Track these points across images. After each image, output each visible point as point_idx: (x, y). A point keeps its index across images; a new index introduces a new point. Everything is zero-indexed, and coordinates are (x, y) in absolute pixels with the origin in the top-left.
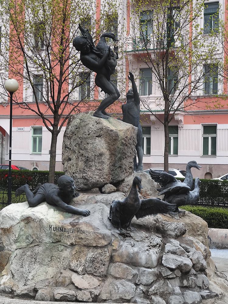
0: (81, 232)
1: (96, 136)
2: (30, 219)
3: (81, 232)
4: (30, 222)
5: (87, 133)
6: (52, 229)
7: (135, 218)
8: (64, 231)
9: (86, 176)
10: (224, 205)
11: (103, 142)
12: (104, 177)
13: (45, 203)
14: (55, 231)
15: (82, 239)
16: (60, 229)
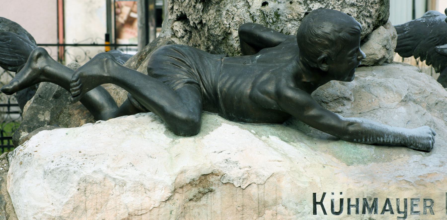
8: (380, 210)
16: (365, 205)
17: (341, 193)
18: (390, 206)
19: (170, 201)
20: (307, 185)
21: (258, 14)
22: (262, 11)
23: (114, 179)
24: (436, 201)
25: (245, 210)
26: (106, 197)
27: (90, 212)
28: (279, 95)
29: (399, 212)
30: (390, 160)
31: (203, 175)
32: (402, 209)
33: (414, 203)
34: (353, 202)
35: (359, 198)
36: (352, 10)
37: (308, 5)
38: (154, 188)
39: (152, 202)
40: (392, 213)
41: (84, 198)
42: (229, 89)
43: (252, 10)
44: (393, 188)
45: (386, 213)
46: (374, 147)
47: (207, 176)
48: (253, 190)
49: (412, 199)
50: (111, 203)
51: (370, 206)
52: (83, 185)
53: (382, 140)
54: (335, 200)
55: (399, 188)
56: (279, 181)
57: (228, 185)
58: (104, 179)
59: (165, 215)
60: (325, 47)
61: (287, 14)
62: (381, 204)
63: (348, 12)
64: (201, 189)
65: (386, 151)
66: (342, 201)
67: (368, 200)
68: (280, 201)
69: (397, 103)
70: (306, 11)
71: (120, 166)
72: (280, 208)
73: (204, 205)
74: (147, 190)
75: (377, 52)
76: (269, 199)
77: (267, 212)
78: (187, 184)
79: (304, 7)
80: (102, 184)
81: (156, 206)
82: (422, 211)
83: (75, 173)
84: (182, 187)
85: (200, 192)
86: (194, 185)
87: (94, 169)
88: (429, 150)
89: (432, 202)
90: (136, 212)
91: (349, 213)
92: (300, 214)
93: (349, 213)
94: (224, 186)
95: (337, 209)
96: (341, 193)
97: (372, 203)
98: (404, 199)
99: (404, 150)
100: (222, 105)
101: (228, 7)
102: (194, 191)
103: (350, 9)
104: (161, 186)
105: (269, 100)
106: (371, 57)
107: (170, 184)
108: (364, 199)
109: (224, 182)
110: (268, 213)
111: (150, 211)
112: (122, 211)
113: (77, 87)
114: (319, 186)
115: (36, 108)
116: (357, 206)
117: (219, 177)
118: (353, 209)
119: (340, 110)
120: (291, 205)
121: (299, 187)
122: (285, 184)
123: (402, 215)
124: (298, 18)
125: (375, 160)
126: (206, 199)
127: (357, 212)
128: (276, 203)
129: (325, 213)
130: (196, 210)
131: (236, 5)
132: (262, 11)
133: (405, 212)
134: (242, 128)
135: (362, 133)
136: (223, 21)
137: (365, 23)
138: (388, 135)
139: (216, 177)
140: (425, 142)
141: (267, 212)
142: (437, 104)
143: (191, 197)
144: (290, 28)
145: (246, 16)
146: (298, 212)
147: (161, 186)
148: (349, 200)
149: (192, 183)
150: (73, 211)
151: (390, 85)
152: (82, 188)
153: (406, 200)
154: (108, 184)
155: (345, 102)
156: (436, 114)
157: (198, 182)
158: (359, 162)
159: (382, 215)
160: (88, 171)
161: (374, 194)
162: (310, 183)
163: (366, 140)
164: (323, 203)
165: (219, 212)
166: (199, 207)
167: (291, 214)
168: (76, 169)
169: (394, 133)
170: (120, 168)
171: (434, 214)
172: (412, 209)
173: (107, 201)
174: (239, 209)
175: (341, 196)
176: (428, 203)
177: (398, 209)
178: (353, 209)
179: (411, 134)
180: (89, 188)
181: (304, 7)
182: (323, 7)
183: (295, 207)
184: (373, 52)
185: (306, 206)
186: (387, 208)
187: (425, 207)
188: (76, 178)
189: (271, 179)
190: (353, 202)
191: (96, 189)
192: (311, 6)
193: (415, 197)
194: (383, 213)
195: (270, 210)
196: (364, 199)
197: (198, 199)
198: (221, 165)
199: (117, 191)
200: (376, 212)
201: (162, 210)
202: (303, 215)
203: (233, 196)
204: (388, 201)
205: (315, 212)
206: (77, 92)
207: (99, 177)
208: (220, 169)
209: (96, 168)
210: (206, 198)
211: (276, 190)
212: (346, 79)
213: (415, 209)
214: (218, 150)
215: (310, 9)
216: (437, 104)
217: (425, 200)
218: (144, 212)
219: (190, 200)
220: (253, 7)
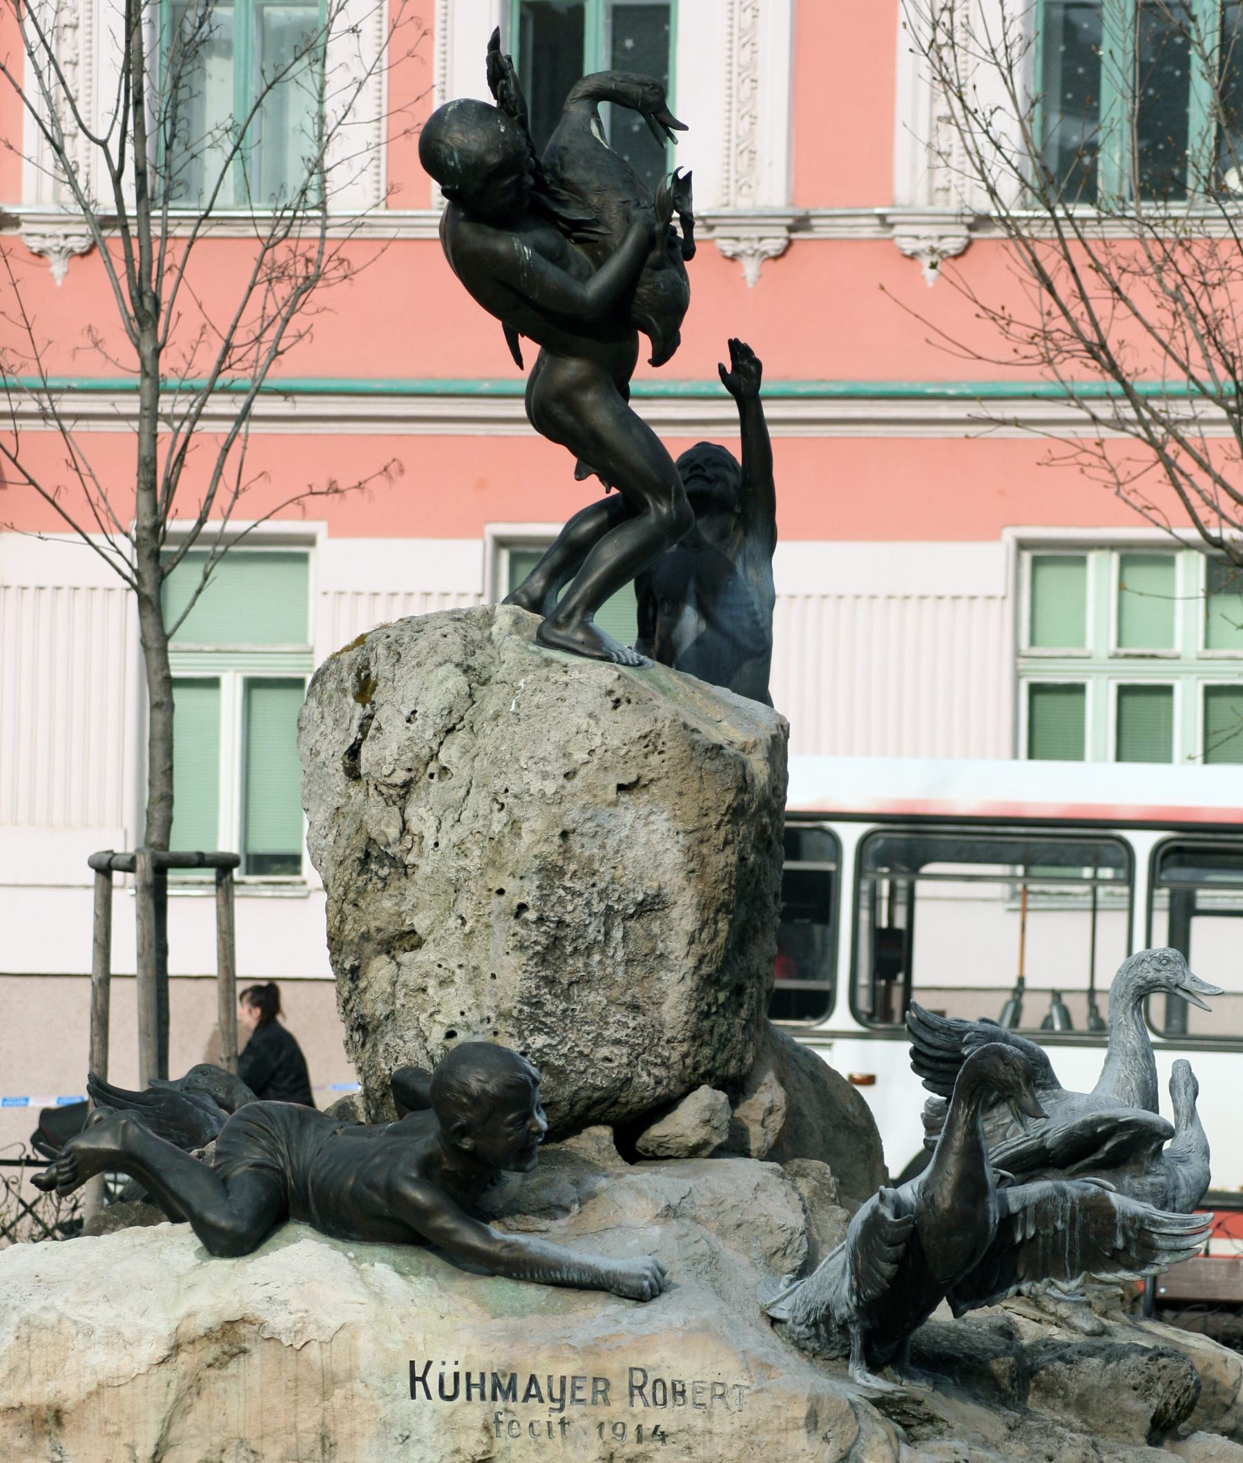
0: (660, 1395)
1: (621, 788)
3: (660, 1395)
4: (244, 1351)
5: (557, 768)
6: (434, 1389)
7: (942, 1313)
8: (521, 1394)
9: (549, 1045)
11: (661, 823)
12: (660, 1056)
15: (663, 1437)
16: (496, 1385)
17: (456, 1363)
18: (538, 1388)
19: (169, 1365)
20: (401, 1346)
21: (439, 1052)
22: (445, 1047)
23: (75, 1322)
24: (613, 1382)
25: (300, 1388)
26: (62, 1353)
27: (37, 1377)
28: (392, 1193)
29: (553, 1400)
30: (566, 1311)
32: (557, 1395)
33: (578, 1384)
34: (475, 1379)
36: (616, 1051)
37: (525, 1039)
38: (140, 1340)
39: (135, 1365)
40: (541, 1401)
41: (26, 1352)
42: (324, 1179)
43: (430, 1046)
44: (543, 1356)
45: (531, 1400)
46: (550, 1289)
48: (313, 1352)
49: (574, 1378)
50: (71, 1364)
51: (505, 1387)
52: (24, 1331)
53: (558, 1275)
54: (445, 1376)
55: (555, 1358)
56: (354, 1337)
57: (272, 1342)
58: (59, 1321)
59: (158, 1389)
60: (463, 1108)
63: (607, 1054)
64: (227, 1348)
65: (570, 1296)
66: (456, 1375)
67: (499, 1375)
68: (356, 1374)
69: (648, 1218)
70: (522, 1049)
71: (86, 1299)
72: (358, 1386)
73: (233, 1376)
74: (127, 1344)
75: (688, 1132)
76: (340, 1368)
77: (337, 1392)
78: (201, 1338)
79: (519, 1043)
80: (56, 1330)
82: (589, 1400)
83: (14, 1309)
84: (192, 1342)
85: (224, 1353)
87: (43, 1303)
89: (607, 1383)
90: (110, 1381)
91: (469, 1398)
92: (389, 1398)
93: (469, 1398)
94: (266, 1344)
95: (449, 1391)
96: (456, 1363)
97: (507, 1381)
99: (601, 1296)
100: (313, 1208)
101: (387, 1039)
102: (214, 1350)
103: (612, 1048)
104: (150, 1337)
105: (377, 1198)
106: (679, 1140)
107: (166, 1334)
108: (494, 1374)
109: (266, 1336)
110: (339, 1393)
111: (133, 1379)
112: (88, 1378)
113: (66, 1169)
114: (421, 1348)
115: (104, 1218)
117: (256, 1328)
118: (475, 1392)
119: (543, 1228)
120: (374, 1381)
121: (387, 1349)
122: (364, 1343)
123: (557, 1405)
125: (541, 1311)
127: (483, 1397)
128: (350, 1377)
129: (429, 1397)
130: (221, 1384)
132: (445, 1047)
133: (562, 1400)
134: (334, 1247)
135: (524, 1262)
136: (379, 1063)
138: (569, 1267)
140: (634, 1282)
141: (337, 1392)
142: (739, 1226)
143: (210, 1360)
145: (419, 1055)
147: (150, 1337)
148: (468, 1375)
149: (208, 1336)
150: (9, 1375)
151: (645, 1186)
152: (24, 1335)
154: (65, 1331)
155: (559, 1213)
156: (733, 1245)
157: (219, 1335)
158: (514, 1313)
160: (33, 1307)
161: (510, 1366)
162: (406, 1343)
163: (532, 1276)
164: (428, 1379)
165: (257, 1389)
166: (224, 1378)
167: (375, 1396)
168: (17, 1303)
169: (580, 1264)
170: (85, 1303)
172: (573, 1396)
173: (64, 1360)
174: (291, 1384)
175: (456, 1369)
176: (601, 1386)
177: (551, 1395)
178: (475, 1392)
179: (608, 1269)
180: (34, 1336)
181: (519, 1043)
182: (554, 1043)
183: (380, 1384)
184: (681, 1132)
186: (533, 1392)
187: (595, 1392)
188: (15, 1318)
189: (341, 1334)
190: (475, 1379)
191: (46, 1337)
192: (530, 1041)
193: (579, 1374)
194: (525, 1400)
195: (341, 1388)
196: (494, 1374)
197: (223, 1365)
198: (260, 1307)
199: (79, 1342)
200: (515, 1398)
201: (153, 1379)
202: (394, 1400)
203: (280, 1362)
204: (533, 1379)
205: (413, 1396)
206: (66, 1176)
207: (51, 1318)
208: (257, 1313)
209: (47, 1303)
211: (350, 1354)
212: (512, 1166)
213: (579, 1395)
214: (261, 1281)
215: (528, 1046)
216: (739, 1226)
217: (595, 1380)
218: (122, 1381)
219: (210, 1366)
220: (430, 1039)
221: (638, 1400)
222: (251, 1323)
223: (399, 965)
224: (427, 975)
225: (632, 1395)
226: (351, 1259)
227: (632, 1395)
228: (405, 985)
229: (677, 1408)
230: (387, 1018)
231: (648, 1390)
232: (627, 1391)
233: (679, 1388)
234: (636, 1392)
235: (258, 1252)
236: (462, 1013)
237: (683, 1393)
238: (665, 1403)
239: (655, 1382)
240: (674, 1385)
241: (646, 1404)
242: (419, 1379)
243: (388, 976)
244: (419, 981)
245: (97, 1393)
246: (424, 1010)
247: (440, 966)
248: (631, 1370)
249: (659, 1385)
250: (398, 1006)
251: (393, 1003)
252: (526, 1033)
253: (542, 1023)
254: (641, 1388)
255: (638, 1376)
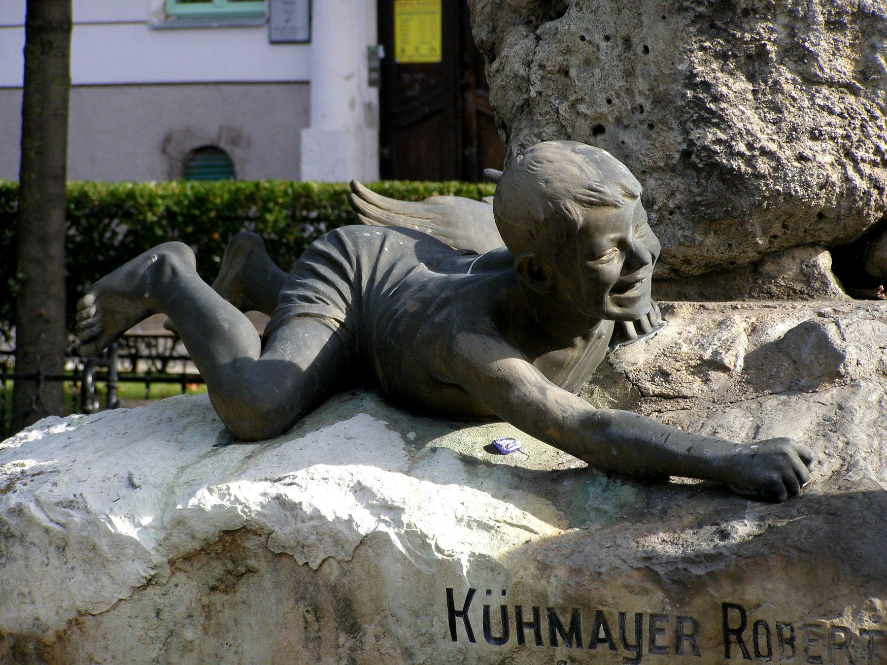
0: (762, 642)
2: (251, 543)
4: (250, 571)
8: (586, 638)
10: (530, 625)
13: (369, 402)
14: (506, 647)
16: (555, 622)
29: (627, 646)
31: (226, 532)
32: (632, 639)
34: (528, 617)
35: (539, 607)
37: (688, 133)
40: (613, 647)
47: (237, 535)
49: (653, 616)
51: (567, 629)
54: (491, 609)
61: (641, 154)
62: (586, 625)
64: (230, 566)
66: (504, 608)
70: (685, 146)
81: (124, 598)
86: (213, 555)
88: (276, 506)
91: (521, 639)
93: (521, 639)
95: (496, 633)
96: (504, 593)
98: (636, 614)
102: (218, 568)
116: (520, 625)
117: (263, 539)
123: (632, 654)
124: (667, 165)
126: (246, 590)
127: (539, 641)
129: (472, 638)
131: (541, 133)
133: (639, 646)
137: (862, 178)
139: (257, 538)
144: (653, 189)
146: (420, 633)
153: (639, 616)
157: (219, 548)
159: (593, 651)
164: (470, 614)
171: (699, 656)
172: (652, 641)
185: (435, 619)
186: (602, 635)
190: (528, 617)
193: (658, 611)
200: (579, 645)
210: (246, 586)
215: (691, 143)
219: (213, 589)
221: (737, 652)
222: (255, 533)
223: (538, 38)
224: (568, 51)
225: (727, 642)
226: (408, 442)
227: (727, 642)
228: (542, 66)
229: (784, 661)
230: (521, 109)
231: (747, 634)
232: (721, 637)
233: (787, 633)
234: (733, 638)
235: (288, 434)
236: (609, 101)
237: (791, 641)
238: (770, 654)
239: (756, 624)
240: (779, 630)
241: (746, 656)
242: (459, 614)
243: (522, 54)
244: (560, 59)
245: (76, 623)
246: (565, 98)
247: (583, 38)
248: (726, 606)
249: (761, 629)
250: (533, 93)
251: (528, 90)
252: (690, 125)
253: (710, 111)
254: (739, 632)
255: (734, 614)
